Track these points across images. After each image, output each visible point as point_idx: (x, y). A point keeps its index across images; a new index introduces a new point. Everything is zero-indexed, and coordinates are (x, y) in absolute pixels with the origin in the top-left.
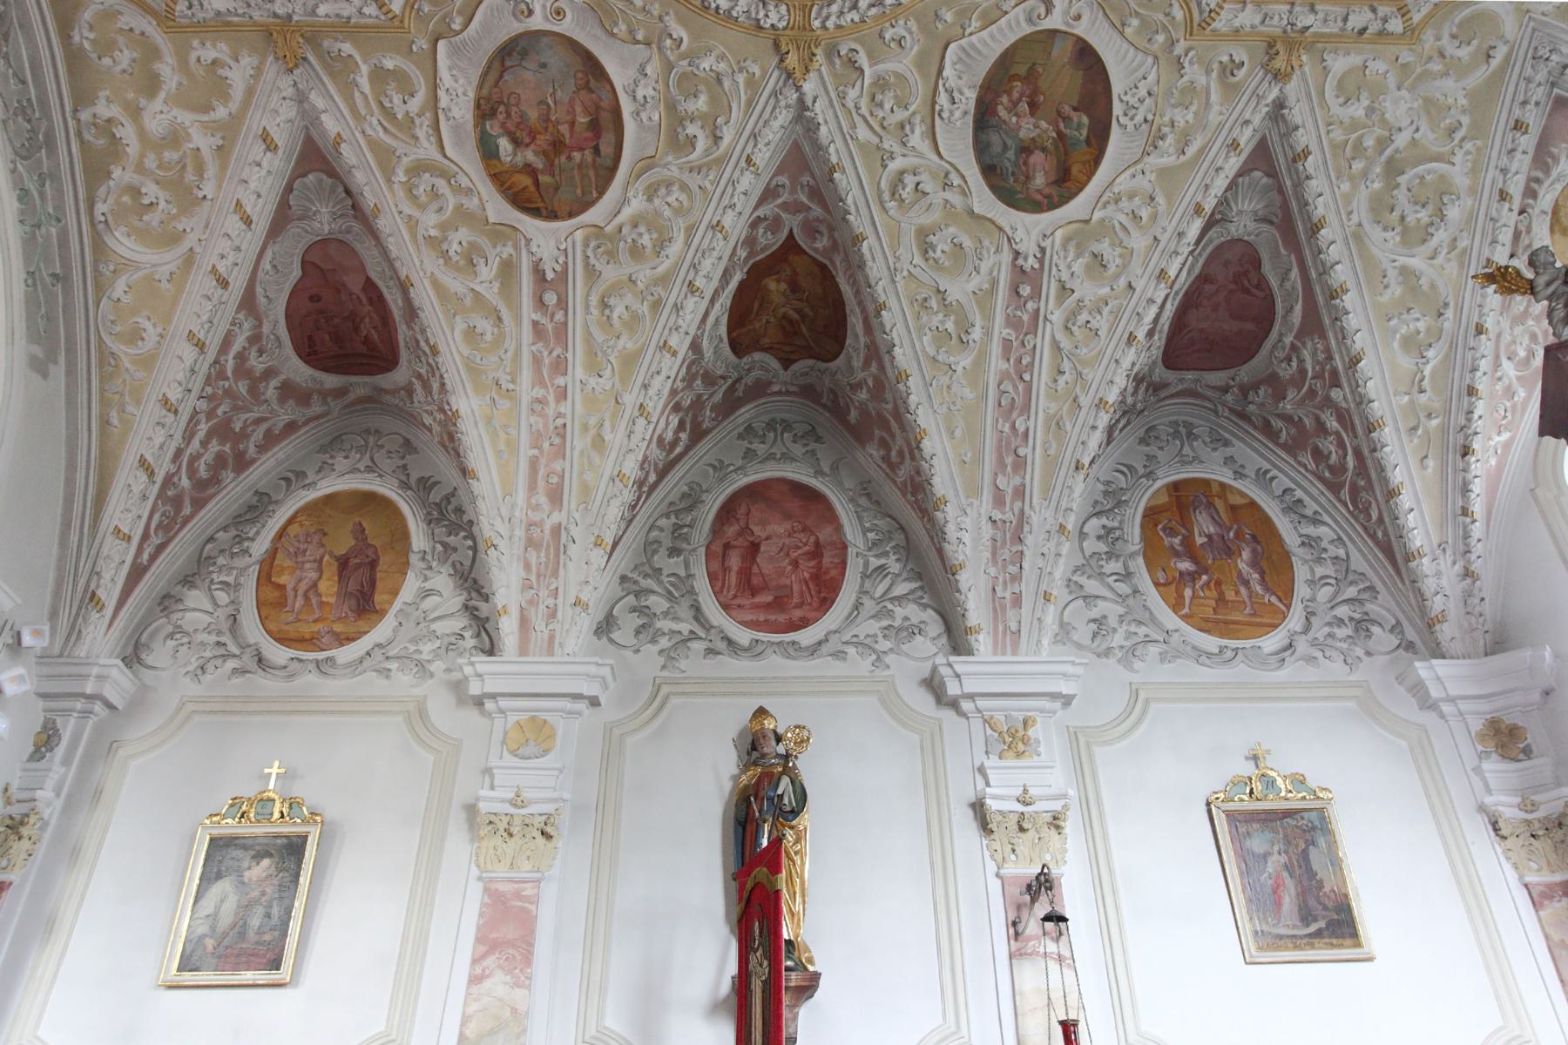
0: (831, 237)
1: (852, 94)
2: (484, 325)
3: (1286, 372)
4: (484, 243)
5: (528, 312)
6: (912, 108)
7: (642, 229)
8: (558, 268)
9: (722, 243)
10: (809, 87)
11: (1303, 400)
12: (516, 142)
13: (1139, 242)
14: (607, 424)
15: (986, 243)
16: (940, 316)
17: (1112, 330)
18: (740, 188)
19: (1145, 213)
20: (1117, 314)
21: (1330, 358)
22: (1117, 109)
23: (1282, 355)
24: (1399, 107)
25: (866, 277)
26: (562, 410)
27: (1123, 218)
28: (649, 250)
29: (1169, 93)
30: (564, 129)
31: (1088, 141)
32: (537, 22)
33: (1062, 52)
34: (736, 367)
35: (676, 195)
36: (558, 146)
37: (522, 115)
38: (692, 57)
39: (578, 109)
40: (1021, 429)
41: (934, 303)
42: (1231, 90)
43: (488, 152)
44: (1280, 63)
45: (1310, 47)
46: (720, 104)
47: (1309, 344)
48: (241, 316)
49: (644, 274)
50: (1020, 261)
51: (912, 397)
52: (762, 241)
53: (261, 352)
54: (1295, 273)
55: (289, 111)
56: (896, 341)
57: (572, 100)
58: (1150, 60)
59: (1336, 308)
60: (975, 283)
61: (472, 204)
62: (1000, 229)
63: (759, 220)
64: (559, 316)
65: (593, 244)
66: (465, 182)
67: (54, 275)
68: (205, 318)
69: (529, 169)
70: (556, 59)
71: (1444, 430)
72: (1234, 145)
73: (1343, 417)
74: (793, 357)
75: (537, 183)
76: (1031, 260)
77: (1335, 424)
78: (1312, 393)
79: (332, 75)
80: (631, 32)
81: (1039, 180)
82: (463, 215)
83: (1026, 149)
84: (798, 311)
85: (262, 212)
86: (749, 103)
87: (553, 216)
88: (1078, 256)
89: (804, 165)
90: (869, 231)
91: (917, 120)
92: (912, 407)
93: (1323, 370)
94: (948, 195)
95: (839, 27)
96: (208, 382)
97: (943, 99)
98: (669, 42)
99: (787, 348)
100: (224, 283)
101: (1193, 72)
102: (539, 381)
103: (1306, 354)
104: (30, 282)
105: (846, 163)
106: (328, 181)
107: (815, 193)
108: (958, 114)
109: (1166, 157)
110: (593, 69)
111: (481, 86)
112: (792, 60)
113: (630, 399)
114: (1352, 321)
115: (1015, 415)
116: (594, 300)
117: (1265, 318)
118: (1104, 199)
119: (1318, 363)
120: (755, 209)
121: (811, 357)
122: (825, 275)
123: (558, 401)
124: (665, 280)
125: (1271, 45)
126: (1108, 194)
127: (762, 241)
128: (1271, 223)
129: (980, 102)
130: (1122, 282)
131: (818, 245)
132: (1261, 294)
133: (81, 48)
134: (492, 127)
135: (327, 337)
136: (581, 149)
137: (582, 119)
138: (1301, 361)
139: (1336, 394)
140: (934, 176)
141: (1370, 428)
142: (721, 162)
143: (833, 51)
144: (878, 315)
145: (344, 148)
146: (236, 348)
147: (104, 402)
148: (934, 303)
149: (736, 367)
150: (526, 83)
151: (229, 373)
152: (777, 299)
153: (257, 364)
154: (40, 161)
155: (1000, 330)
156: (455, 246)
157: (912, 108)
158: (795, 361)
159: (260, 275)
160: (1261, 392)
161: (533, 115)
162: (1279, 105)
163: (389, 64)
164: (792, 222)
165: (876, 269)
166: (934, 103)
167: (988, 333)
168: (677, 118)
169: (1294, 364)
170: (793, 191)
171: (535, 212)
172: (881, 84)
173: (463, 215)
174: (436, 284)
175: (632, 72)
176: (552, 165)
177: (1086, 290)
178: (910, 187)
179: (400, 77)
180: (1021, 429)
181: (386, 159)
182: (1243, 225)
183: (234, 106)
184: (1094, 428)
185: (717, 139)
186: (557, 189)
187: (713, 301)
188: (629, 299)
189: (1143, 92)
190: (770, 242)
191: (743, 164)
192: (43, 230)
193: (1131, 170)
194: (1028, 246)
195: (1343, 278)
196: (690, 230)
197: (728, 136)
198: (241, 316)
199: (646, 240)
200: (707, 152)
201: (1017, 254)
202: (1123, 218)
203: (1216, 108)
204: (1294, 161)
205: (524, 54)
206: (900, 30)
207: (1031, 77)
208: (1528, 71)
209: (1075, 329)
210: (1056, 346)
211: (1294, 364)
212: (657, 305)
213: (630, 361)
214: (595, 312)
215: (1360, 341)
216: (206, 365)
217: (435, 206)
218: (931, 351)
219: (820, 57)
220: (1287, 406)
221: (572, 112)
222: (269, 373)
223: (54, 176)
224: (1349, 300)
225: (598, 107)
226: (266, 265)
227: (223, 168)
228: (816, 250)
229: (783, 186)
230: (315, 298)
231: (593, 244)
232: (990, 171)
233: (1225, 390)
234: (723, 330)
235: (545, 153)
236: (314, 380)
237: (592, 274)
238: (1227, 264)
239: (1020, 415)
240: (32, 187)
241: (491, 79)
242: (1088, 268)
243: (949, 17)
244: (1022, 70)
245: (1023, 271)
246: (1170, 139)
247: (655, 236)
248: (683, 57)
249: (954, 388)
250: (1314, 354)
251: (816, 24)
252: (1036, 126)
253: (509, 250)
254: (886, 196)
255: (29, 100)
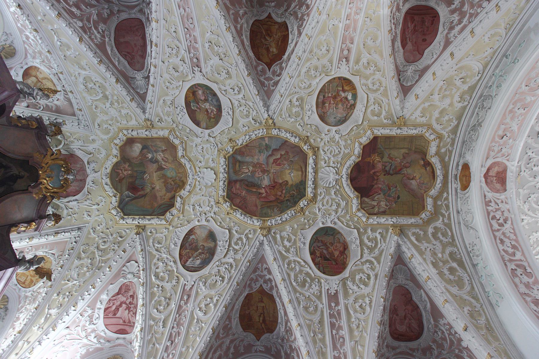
0: (257, 71)
1: (255, 113)
2: (370, 42)
3: (101, 27)
4: (362, 69)
5: (354, 48)
6: (238, 110)
7: (313, 75)
8: (341, 62)
9: (289, 72)
10: (266, 116)
11: (90, 16)
12: (346, 98)
13: (166, 76)
14: (334, 6)
15: (211, 75)
16: (220, 51)
17: (163, 48)
18: (284, 88)
19: (168, 84)
20: (164, 53)
21: (90, 37)
22: (185, 110)
23: (106, 32)
24: (113, 112)
25: (245, 62)
26: (349, 10)
27: (173, 82)
28: (312, 69)
29: (173, 114)
30: (332, 102)
31: (190, 103)
32: (334, 128)
33: (204, 124)
34: (286, 17)
35: (303, 86)
36: (335, 98)
37: (343, 105)
38: (296, 121)
39: (327, 108)
40: (181, 9)
41: (223, 56)
42: (158, 115)
43: (355, 96)
44: (149, 123)
45: (143, 127)
46: (289, 110)
47: (99, 40)
48: (452, 39)
49: (314, 62)
50: (199, 69)
51: (223, 22)
52: (278, 67)
53: (452, 22)
54: (117, 63)
55: (407, 105)
56: (232, 43)
57: (329, 110)
58: (181, 123)
59: (98, 57)
60: (211, 62)
61: (363, 81)
62: (207, 79)
63: (279, 76)
64: (344, 46)
65: (329, 70)
66: (364, 87)
67: (507, 58)
68: (465, 42)
69: (344, 91)
70: (332, 120)
71: (35, 17)
72: (151, 103)
73: (72, 15)
74: (267, 19)
75: (343, 87)
76: (196, 70)
77: (74, 10)
78: (89, 21)
79: (392, 114)
80: (311, 127)
81: (200, 92)
82: (367, 78)
83: (206, 100)
84: (266, 40)
85: (428, 75)
86: (282, 110)
87: (340, 78)
88: (182, 71)
89: (266, 91)
90: (246, 78)
91: (237, 108)
92: (223, 17)
93: (90, 32)
94: (225, 88)
95: (259, 130)
96: (478, 14)
97: (231, 113)
98: (302, 125)
99: (269, 23)
100: (452, 54)
101: (169, 120)
102: (356, 21)
103: (98, 36)
104: (517, 61)
105: (254, 96)
106: (404, 84)
107: (263, 84)
108: (226, 109)
109: (169, 99)
110: (322, 118)
111: (353, 113)
112: (271, 121)
113: (324, 17)
114: (90, 54)
115: (186, 15)
116: (331, 52)
117: (118, 44)
118: (181, 87)
119: (93, 34)
120: (280, 79)
121: (261, 20)
122: (258, 57)
123: (350, 14)
124: (308, 60)
125: (153, 126)
126: (180, 89)
127: (278, 67)
128: (131, 78)
129: (221, 112)
130: (166, 64)
131: (261, 67)
132: (123, 53)
133: (456, 121)
134: (352, 102)
135: (426, 23)
136: (328, 97)
137: (327, 105)
138: (99, 32)
139: (80, 24)
140: (229, 93)
141: (59, 15)
142: (290, 95)
143: (260, 123)
144: (240, 52)
145: (396, 95)
146: (460, 26)
147: (523, 8)
148: (223, 56)
149: (286, 17)
150: (340, 113)
151: (468, 15)
152: (273, 45)
153: (456, 17)
154: (487, 92)
155: (199, 46)
156: (372, 69)
157: (238, 110)
158: (266, 18)
159: (438, 54)
160: (106, 15)
161: (340, 106)
162: (144, 112)
163: (376, 118)
164: (269, 74)
165: (242, 66)
166: (233, 112)
167: (203, 46)
168: (301, 106)
169: (100, 30)
170: (269, 84)
171: (345, 79)
172: (247, 116)
173: (367, 78)
174: (381, 56)
175: (312, 117)
176: (337, 92)
177: (176, 61)
178: (236, 90)
179: (373, 113)
180: (181, 9)
181: (385, 94)
182: (139, 76)
183: (423, 106)
184: (156, 12)
185: (290, 101)
186: (337, 86)
187: (293, 50)
188: (320, 53)
189: (180, 115)
190: (275, 67)
191: (283, 95)
192: (500, 74)
193: (176, 95)
194: (198, 74)
195: (101, 67)
196: (299, 75)
197: (287, 102)
198: (452, 39)
199: (313, 72)
200: (293, 98)
201: (201, 72)
202: (173, 82)
203: (160, 111)
204: (133, 98)
205: (339, 121)
206: (244, 129)
207: (210, 118)
208: (87, 122)
209: (176, 48)
210: (180, 42)
211: (100, 30)
212: (311, 52)
213: (322, 32)
214: (332, 48)
215: (83, 48)
216: (474, 22)
217: (374, 80)
218: (219, 38)
219: (264, 122)
220: (94, 11)
221: (329, 107)
222: (453, 12)
223: (486, 87)
224: (95, 61)
225: (322, 108)
226: (435, 57)
227: (433, 90)
228: (262, 65)
229: (272, 86)
230: (424, 40)
231: (329, 70)
232: (215, 95)
233: (119, 11)
234: (290, 37)
235: (339, 95)
236: (438, 5)
237: (331, 61)
238: (138, 62)
239: (184, 15)
240: (494, 87)
241: (350, 114)
242: (178, 68)
243: (233, 133)
244: (212, 120)
245: (197, 66)
246: (169, 103)
247: (310, 73)
248: (299, 121)
249: (209, 26)
250: (96, 36)
251: (265, 130)
252: (205, 106)
253: (355, 68)
254: (242, 88)
255: (479, 108)
